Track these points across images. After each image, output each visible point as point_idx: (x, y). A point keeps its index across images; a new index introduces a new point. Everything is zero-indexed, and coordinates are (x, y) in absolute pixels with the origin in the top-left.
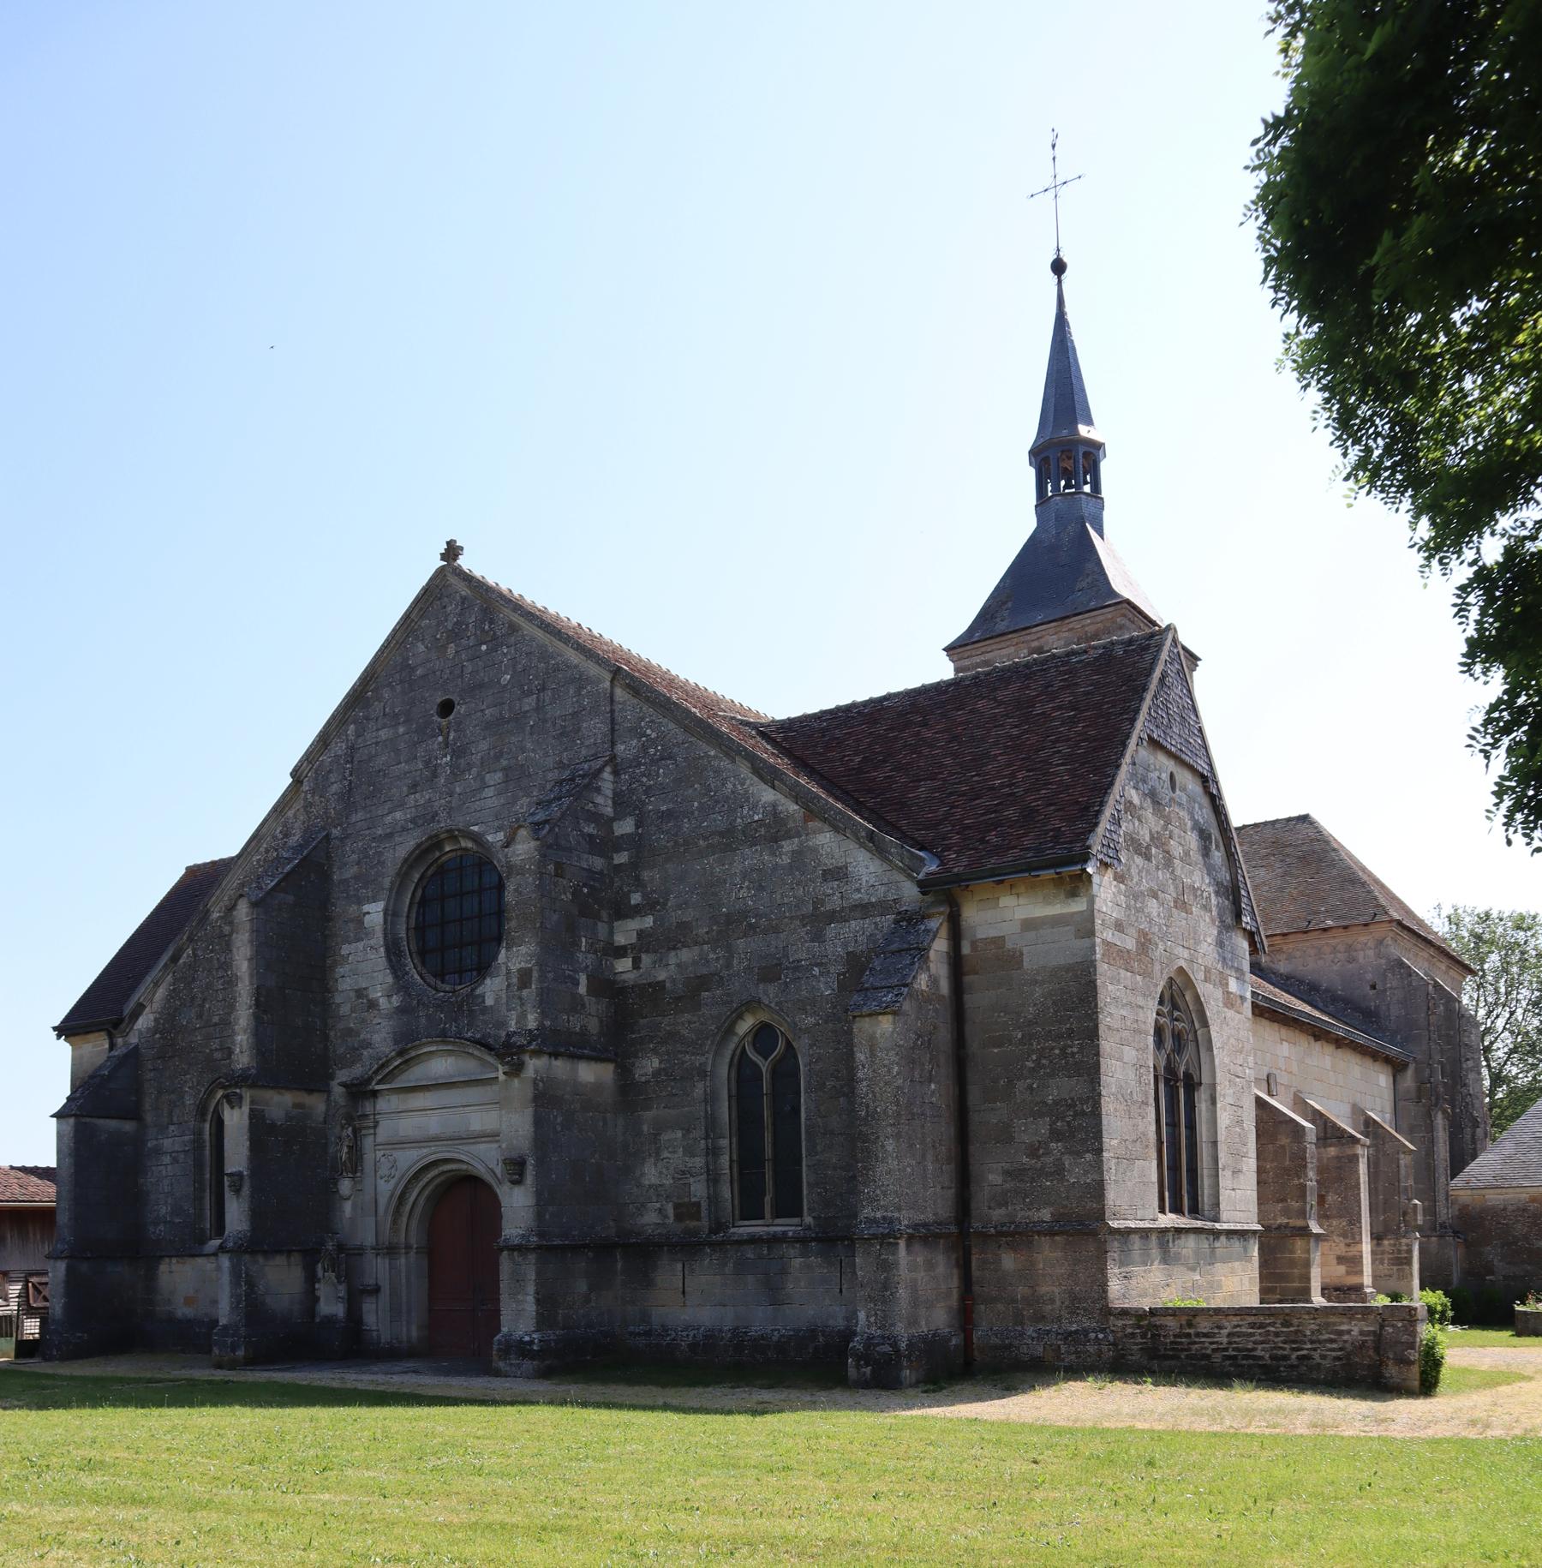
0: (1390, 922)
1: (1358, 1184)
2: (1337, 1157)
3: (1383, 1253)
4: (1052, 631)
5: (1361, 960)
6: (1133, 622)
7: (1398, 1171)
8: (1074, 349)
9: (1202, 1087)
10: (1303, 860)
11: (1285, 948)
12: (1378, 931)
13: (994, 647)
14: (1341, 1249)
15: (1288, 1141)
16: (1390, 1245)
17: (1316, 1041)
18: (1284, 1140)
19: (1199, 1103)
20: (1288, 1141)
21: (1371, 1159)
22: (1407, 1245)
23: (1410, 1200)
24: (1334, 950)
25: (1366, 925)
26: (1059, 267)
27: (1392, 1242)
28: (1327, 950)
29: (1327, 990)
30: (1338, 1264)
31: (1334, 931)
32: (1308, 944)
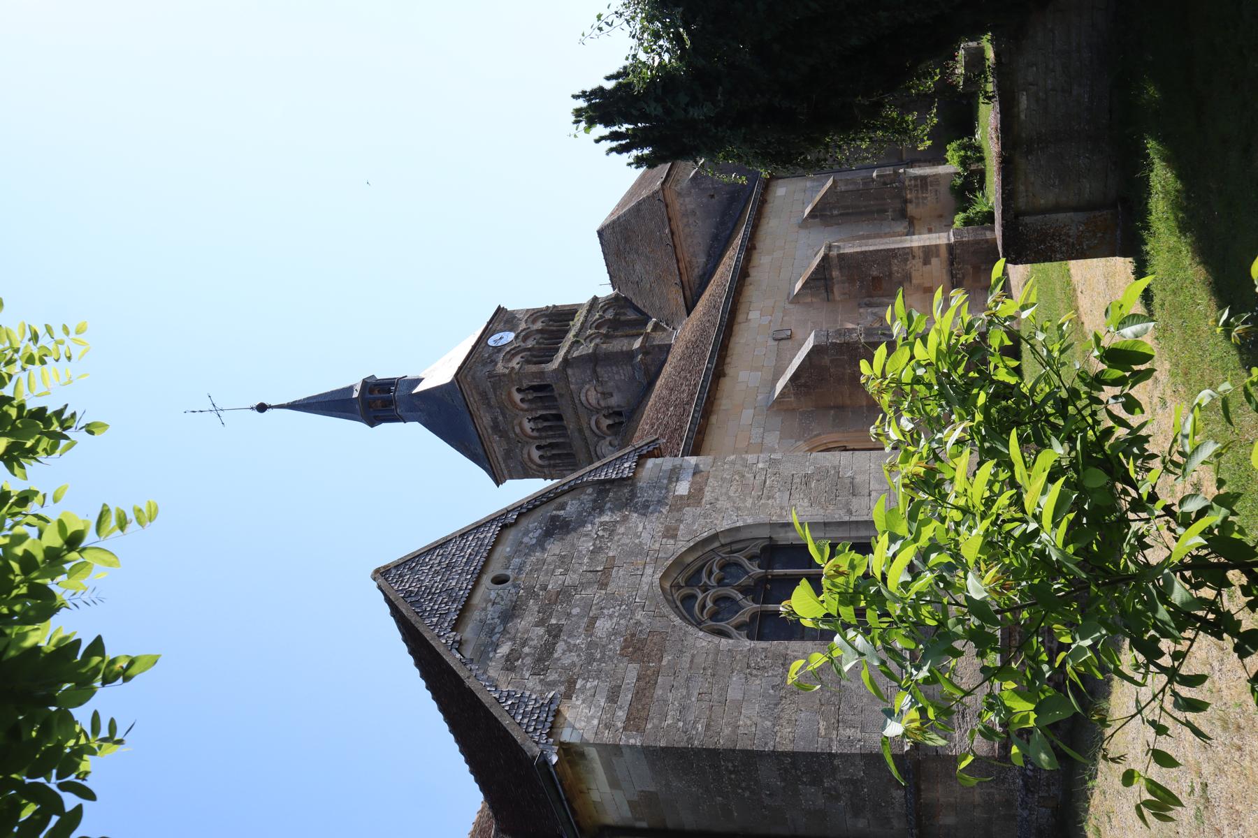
0: (663, 190)
1: (862, 252)
2: (840, 269)
3: (917, 198)
4: (480, 421)
5: (693, 207)
6: (470, 368)
7: (852, 191)
8: (308, 398)
9: (774, 536)
10: (627, 239)
11: (688, 259)
12: (670, 197)
13: (494, 456)
14: (917, 263)
15: (826, 357)
16: (911, 193)
17: (749, 276)
18: (826, 360)
19: (788, 540)
20: (826, 357)
21: (827, 438)
22: (910, 180)
23: (873, 180)
24: (687, 225)
25: (667, 206)
26: (262, 408)
27: (908, 192)
28: (687, 230)
29: (717, 228)
30: (930, 264)
31: (673, 227)
32: (684, 244)
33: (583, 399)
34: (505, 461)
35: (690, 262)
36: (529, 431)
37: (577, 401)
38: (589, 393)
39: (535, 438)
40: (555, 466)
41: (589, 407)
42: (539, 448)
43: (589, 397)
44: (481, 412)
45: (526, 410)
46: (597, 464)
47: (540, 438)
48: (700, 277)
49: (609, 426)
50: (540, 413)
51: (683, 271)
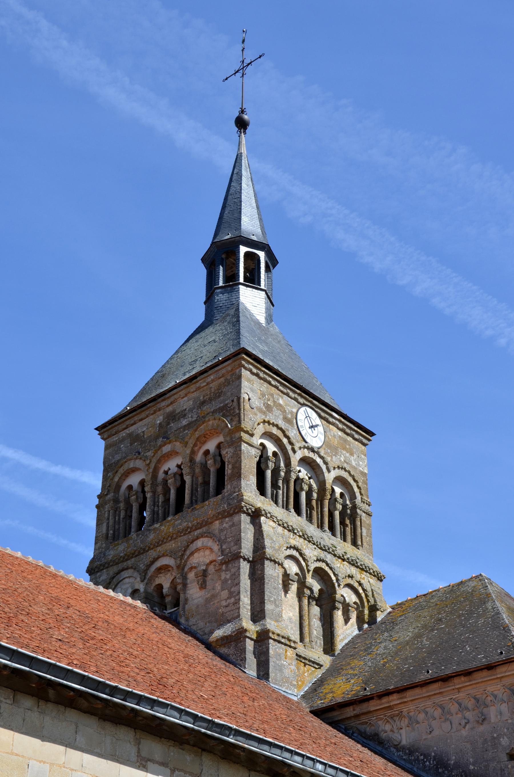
31: (456, 680)
32: (429, 703)
33: (199, 543)
34: (130, 435)
35: (400, 715)
36: (165, 468)
37: (196, 533)
38: (207, 552)
39: (155, 476)
40: (116, 510)
41: (188, 553)
42: (142, 483)
43: (201, 553)
44: (195, 395)
45: (192, 460)
46: (473, 682)
47: (154, 485)
48: (377, 735)
49: (160, 587)
50: (188, 479)
51: (385, 702)
